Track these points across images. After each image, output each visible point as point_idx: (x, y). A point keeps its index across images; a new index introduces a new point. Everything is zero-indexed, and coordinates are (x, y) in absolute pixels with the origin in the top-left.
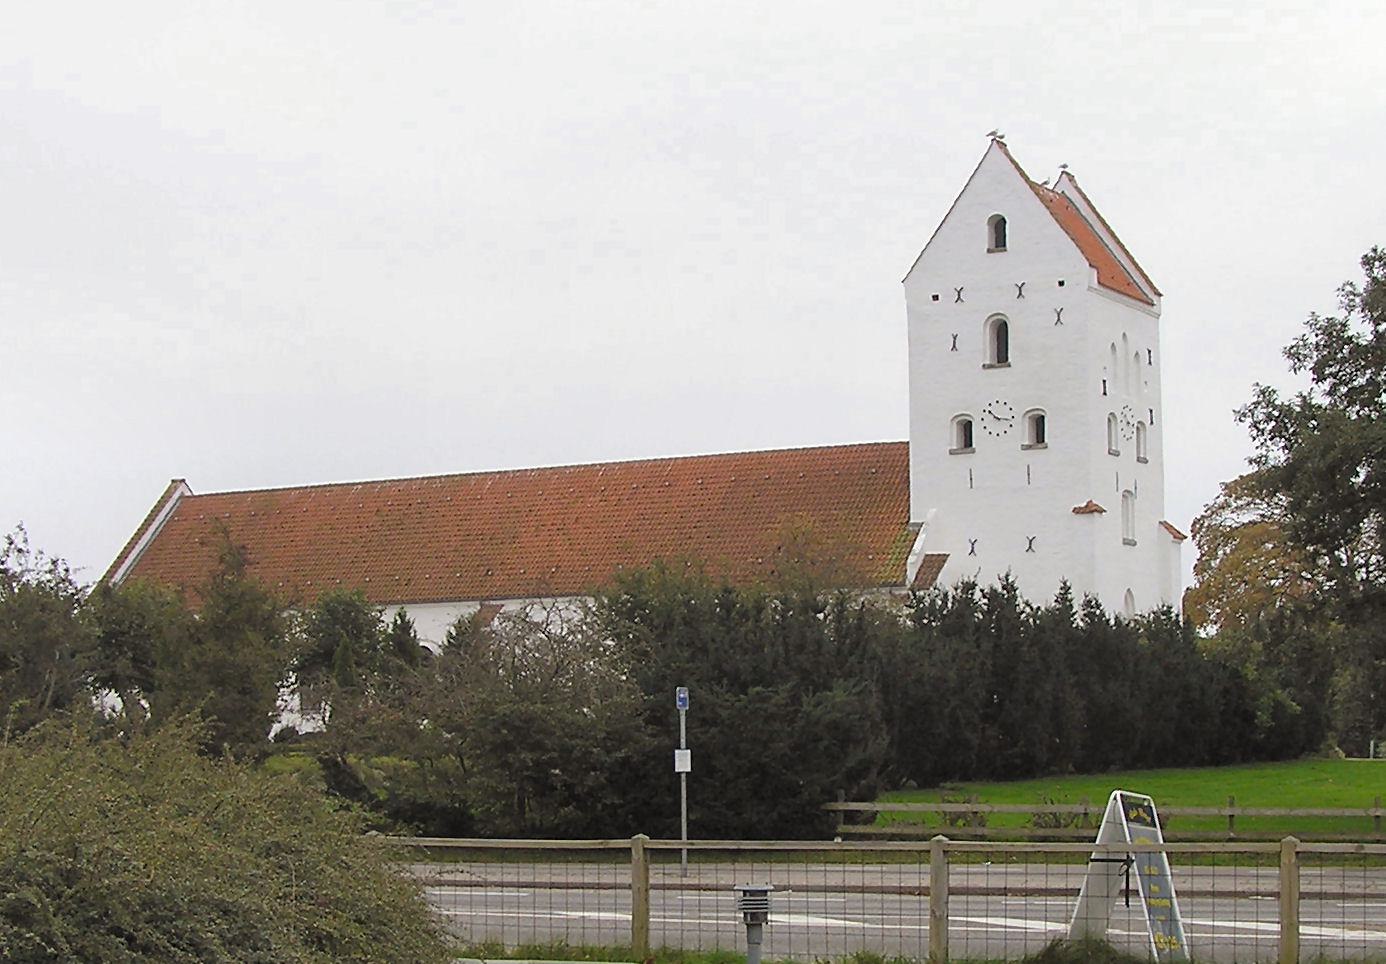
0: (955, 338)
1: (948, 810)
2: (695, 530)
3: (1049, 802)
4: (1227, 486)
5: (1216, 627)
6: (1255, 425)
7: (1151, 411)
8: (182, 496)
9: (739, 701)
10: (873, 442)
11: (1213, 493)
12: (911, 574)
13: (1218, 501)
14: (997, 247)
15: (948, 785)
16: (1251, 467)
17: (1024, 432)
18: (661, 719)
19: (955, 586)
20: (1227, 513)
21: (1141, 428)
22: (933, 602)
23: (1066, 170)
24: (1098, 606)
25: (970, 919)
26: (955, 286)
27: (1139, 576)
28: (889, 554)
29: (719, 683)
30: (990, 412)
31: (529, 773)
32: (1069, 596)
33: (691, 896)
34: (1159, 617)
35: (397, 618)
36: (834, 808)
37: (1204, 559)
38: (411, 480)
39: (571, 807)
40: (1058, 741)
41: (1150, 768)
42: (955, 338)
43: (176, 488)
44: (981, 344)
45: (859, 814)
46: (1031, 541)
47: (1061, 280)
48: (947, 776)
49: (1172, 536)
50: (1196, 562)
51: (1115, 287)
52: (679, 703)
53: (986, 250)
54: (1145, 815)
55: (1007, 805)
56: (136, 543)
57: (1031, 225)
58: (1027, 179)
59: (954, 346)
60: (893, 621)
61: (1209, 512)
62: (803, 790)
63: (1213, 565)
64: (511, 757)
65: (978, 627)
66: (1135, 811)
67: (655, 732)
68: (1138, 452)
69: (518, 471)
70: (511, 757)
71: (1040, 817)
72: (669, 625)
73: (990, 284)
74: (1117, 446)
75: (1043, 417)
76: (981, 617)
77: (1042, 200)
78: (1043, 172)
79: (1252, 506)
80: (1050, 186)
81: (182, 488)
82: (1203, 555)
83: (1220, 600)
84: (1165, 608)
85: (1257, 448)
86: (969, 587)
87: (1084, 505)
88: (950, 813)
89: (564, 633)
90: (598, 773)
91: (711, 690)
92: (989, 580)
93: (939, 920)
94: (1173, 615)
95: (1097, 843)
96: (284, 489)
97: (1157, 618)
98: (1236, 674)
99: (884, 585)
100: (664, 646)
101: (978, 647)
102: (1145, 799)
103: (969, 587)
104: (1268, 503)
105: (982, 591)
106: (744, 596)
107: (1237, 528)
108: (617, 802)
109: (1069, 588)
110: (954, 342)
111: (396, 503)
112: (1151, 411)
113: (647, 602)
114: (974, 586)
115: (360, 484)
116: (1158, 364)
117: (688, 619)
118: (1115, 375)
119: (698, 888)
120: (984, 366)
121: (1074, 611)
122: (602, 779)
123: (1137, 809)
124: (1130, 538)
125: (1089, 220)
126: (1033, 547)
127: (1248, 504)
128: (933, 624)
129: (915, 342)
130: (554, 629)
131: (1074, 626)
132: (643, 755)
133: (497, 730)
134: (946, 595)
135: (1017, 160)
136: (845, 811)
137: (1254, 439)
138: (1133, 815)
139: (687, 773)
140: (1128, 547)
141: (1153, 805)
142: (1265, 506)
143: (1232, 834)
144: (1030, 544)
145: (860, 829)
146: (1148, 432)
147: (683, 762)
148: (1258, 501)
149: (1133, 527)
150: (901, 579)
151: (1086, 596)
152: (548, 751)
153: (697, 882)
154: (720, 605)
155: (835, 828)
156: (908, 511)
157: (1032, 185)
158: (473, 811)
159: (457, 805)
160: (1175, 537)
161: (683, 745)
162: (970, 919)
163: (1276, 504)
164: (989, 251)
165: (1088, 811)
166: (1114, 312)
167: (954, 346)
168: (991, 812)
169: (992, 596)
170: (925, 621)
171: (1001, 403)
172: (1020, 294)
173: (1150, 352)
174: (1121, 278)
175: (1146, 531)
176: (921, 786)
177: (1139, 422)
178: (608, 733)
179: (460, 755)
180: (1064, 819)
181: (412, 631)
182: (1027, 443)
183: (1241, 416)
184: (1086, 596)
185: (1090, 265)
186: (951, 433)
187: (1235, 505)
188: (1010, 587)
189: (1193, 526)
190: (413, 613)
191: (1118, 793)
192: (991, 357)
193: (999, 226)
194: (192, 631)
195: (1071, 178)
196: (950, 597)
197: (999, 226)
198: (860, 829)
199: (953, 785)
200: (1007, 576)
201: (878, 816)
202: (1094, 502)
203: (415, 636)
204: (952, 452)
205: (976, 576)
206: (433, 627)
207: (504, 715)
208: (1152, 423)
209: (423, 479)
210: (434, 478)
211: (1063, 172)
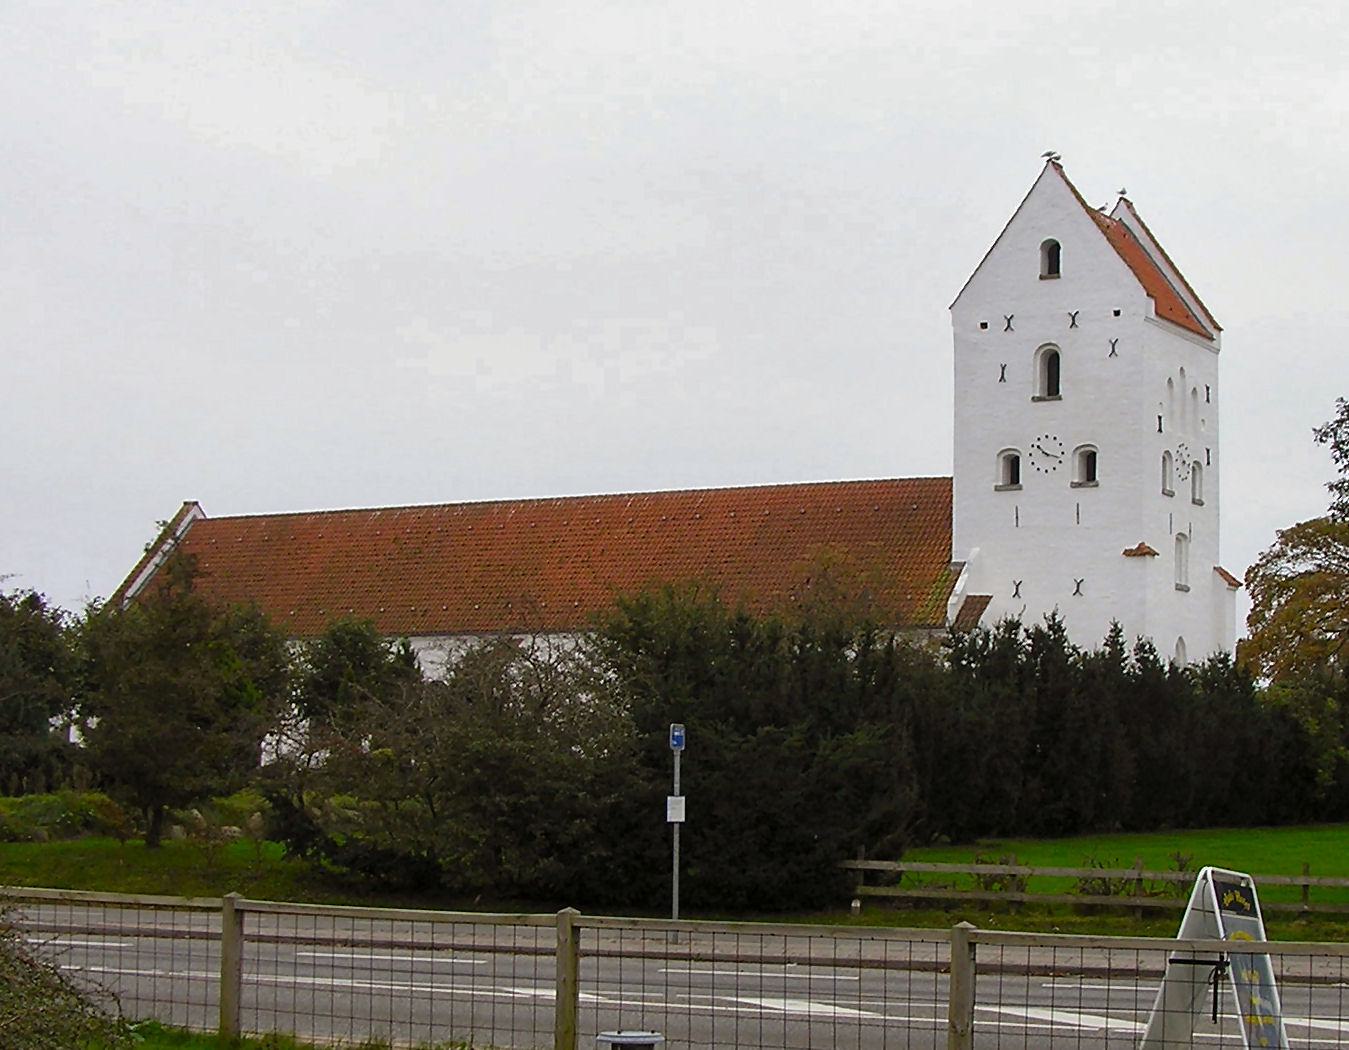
0: (1003, 369)
1: (982, 872)
2: (725, 565)
3: (1098, 866)
4: (1283, 534)
5: (1268, 681)
6: (1336, 446)
7: (1208, 451)
8: (194, 519)
9: (747, 741)
10: (914, 477)
11: (1269, 542)
12: (952, 614)
13: (1274, 549)
14: (1050, 273)
15: (984, 841)
16: (1332, 493)
17: (1073, 470)
18: (658, 762)
19: (997, 625)
20: (1282, 562)
21: (1197, 468)
22: (973, 641)
23: (1125, 196)
24: (1152, 650)
25: (1004, 1010)
26: (1014, 579)
27: (1194, 623)
28: (929, 594)
29: (725, 721)
30: (1038, 447)
31: (504, 818)
32: (1121, 640)
33: (678, 969)
34: (1215, 665)
35: (401, 648)
36: (855, 867)
37: (1258, 609)
38: (432, 507)
39: (551, 859)
40: (1104, 795)
41: (1202, 826)
42: (1003, 369)
43: (188, 511)
44: (1031, 376)
45: (881, 874)
46: (1078, 584)
47: (1117, 309)
48: (983, 830)
49: (1226, 583)
50: (1250, 613)
51: (1173, 318)
52: (673, 742)
53: (1038, 276)
54: (1242, 900)
55: (1050, 869)
56: (145, 567)
57: (1087, 252)
58: (1083, 203)
59: (1002, 377)
60: (929, 662)
61: (1264, 561)
62: (817, 845)
63: (1267, 616)
64: (484, 801)
65: (1021, 669)
66: (1230, 895)
67: (651, 775)
68: (1194, 494)
69: (543, 500)
70: (484, 801)
71: (1087, 881)
72: (671, 657)
73: (1042, 314)
74: (1171, 486)
75: (1095, 454)
76: (1025, 659)
77: (1099, 225)
78: (1102, 198)
79: (1309, 555)
80: (1107, 213)
81: (194, 511)
82: (1256, 606)
83: (1274, 652)
84: (1222, 656)
85: (1340, 471)
86: (1013, 626)
87: (1135, 547)
88: (985, 875)
89: (552, 661)
90: (584, 820)
91: (716, 729)
92: (1034, 619)
93: (962, 1009)
94: (1230, 663)
95: (1178, 938)
96: (300, 514)
97: (1213, 667)
98: (1297, 728)
99: (923, 627)
100: (666, 678)
101: (1021, 691)
102: (1243, 878)
103: (1013, 626)
104: (1325, 553)
105: (1026, 631)
106: (761, 626)
107: (1292, 578)
108: (604, 854)
109: (1121, 631)
110: (1003, 373)
111: (415, 531)
112: (1208, 451)
113: (652, 630)
114: (1017, 625)
115: (378, 510)
116: (1216, 401)
117: (693, 649)
118: (1172, 413)
119: (688, 957)
120: (1033, 398)
121: (1125, 656)
122: (587, 827)
123: (1232, 891)
124: (1183, 584)
125: (1146, 247)
126: (1080, 590)
127: (1304, 554)
128: (973, 665)
129: (962, 371)
130: (542, 657)
131: (1125, 672)
132: (635, 802)
133: (469, 770)
134: (987, 634)
135: (1073, 183)
136: (865, 870)
137: (1337, 461)
138: (1228, 899)
139: (681, 823)
140: (1180, 592)
141: (1253, 886)
142: (1323, 555)
143: (1306, 907)
144: (1078, 586)
145: (882, 891)
146: (1204, 473)
147: (676, 810)
148: (1315, 550)
149: (1186, 572)
150: (940, 621)
151: (1139, 640)
152: (526, 795)
153: (687, 951)
154: (735, 636)
155: (854, 889)
156: (950, 549)
157: (1089, 210)
158: (440, 860)
159: (425, 853)
160: (1230, 584)
161: (677, 790)
162: (1004, 1010)
163: (1334, 554)
164: (1041, 278)
165: (1142, 876)
166: (1167, 347)
167: (1002, 377)
168: (1031, 875)
169: (1037, 636)
170: (964, 662)
171: (1051, 438)
172: (1073, 323)
173: (1208, 388)
174: (1180, 311)
175: (1200, 577)
176: (953, 843)
177: (1195, 462)
178: (596, 776)
179: (428, 797)
180: (1115, 885)
181: (416, 662)
182: (1076, 481)
183: (1322, 435)
184: (1139, 640)
185: (1148, 295)
186: (997, 470)
187: (1291, 554)
188: (1056, 628)
189: (1247, 574)
190: (416, 644)
191: (1209, 869)
192: (1041, 388)
193: (1052, 251)
194: (132, 649)
195: (1129, 205)
196: (991, 637)
197: (1052, 251)
198: (882, 891)
199: (989, 842)
200: (1054, 615)
201: (903, 877)
202: (1147, 544)
203: (419, 667)
204: (997, 489)
205: (1020, 615)
206: (434, 661)
207: (478, 751)
208: (1208, 463)
209: (444, 506)
210: (456, 505)
211: (1121, 199)
